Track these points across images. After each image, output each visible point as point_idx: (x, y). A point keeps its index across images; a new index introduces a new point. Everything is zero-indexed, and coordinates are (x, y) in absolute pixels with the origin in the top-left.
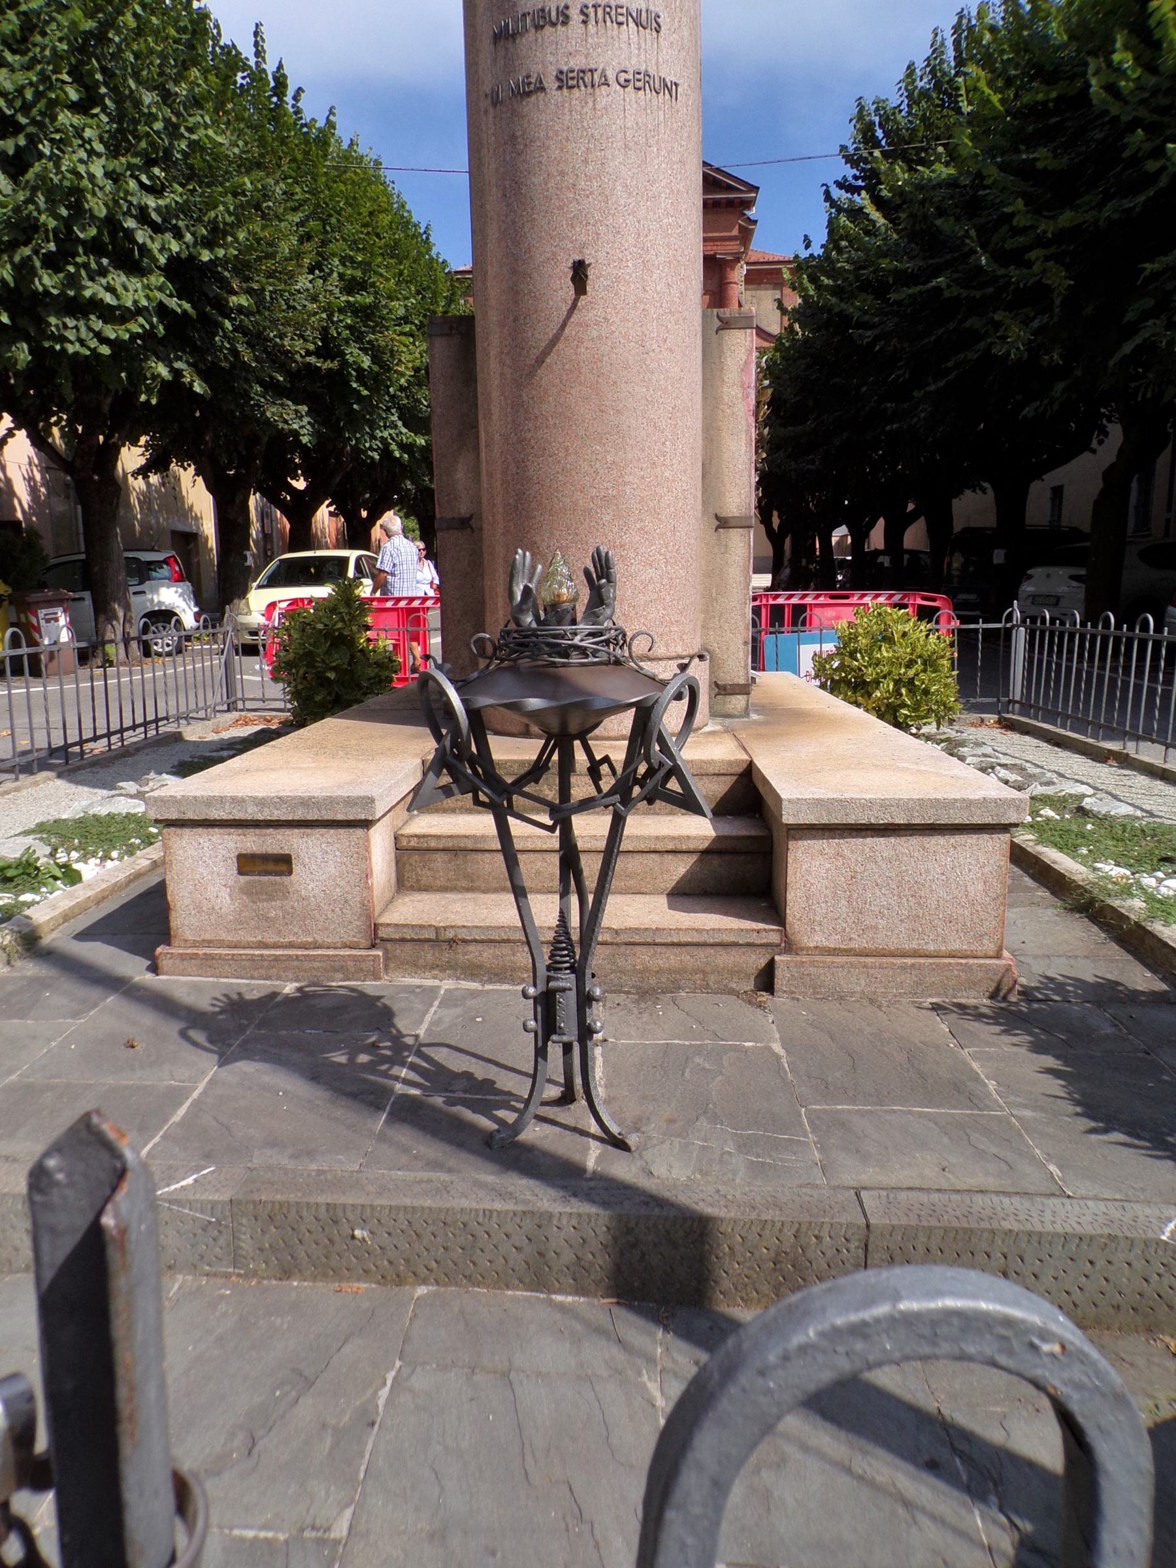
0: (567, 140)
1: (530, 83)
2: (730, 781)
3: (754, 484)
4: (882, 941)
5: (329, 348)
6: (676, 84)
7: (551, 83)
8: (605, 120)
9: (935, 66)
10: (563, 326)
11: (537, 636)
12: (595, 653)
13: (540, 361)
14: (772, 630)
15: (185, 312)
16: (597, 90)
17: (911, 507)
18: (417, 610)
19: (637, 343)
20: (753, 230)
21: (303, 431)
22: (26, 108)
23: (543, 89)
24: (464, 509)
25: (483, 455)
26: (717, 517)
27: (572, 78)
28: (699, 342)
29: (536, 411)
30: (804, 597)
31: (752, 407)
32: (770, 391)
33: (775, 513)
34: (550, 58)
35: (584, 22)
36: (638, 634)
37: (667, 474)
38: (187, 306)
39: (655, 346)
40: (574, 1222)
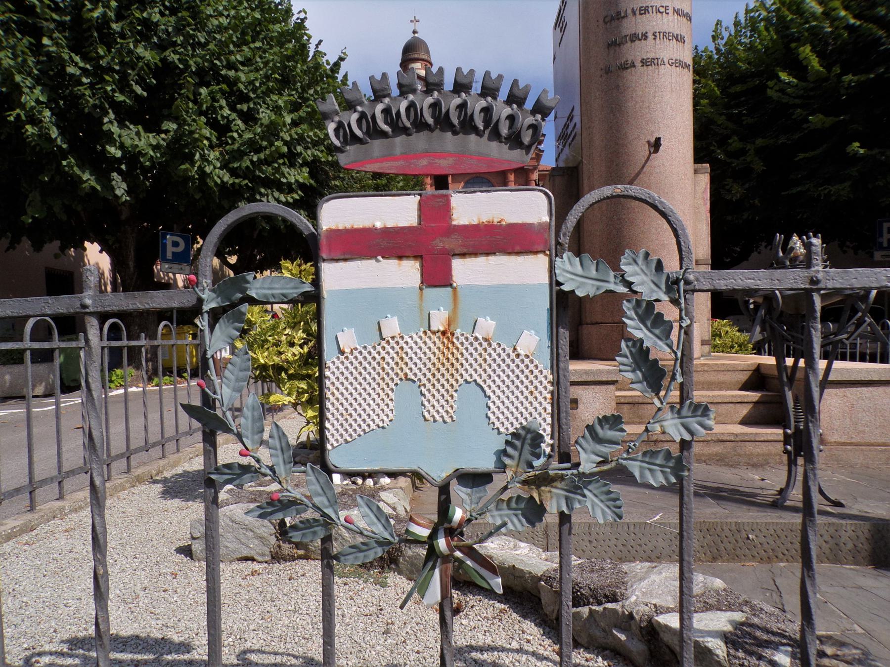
2: (749, 373)
4: (867, 439)
7: (638, 64)
15: (311, 184)
22: (254, 90)
38: (312, 182)
40: (853, 528)
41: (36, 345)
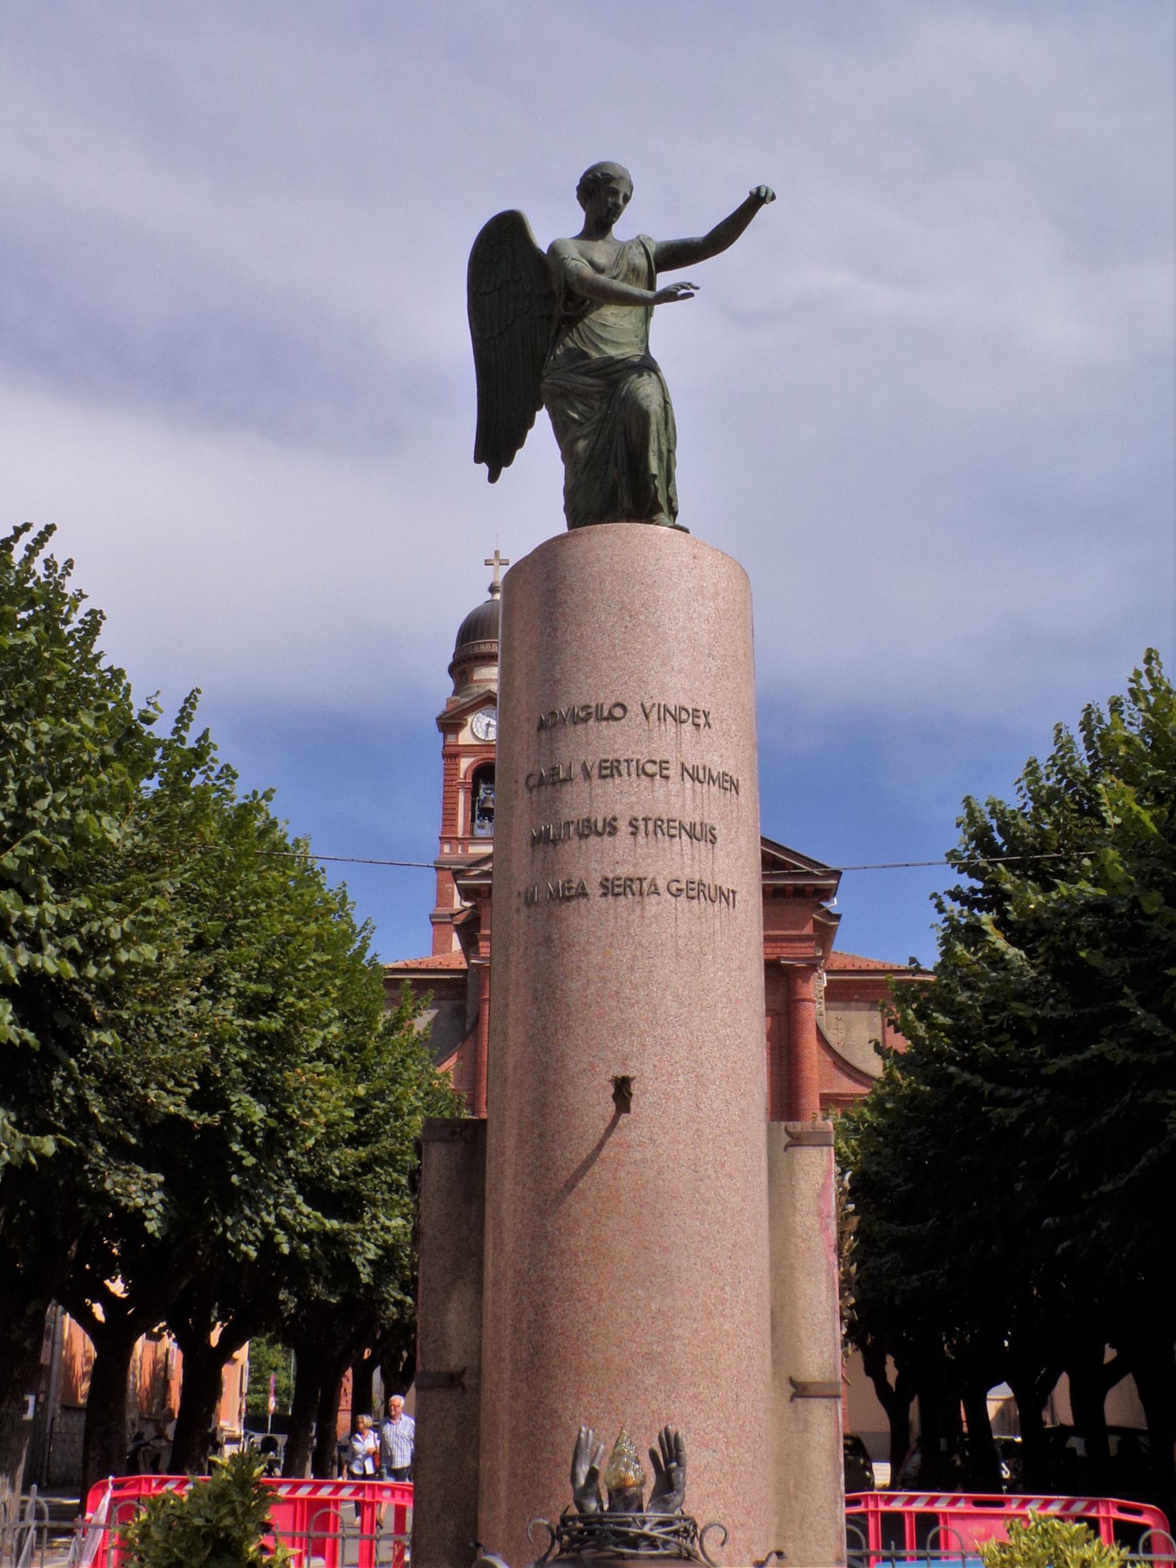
0: (611, 946)
1: (570, 889)
3: (839, 1338)
5: (209, 1097)
6: (733, 892)
7: (594, 890)
8: (654, 928)
9: (1063, 766)
10: (600, 1146)
11: (602, 1524)
12: (666, 1543)
13: (571, 1185)
14: (885, 1553)
15: (25, 1044)
16: (646, 900)
17: (1110, 1354)
18: (325, 1503)
19: (689, 1167)
20: (834, 928)
21: (150, 1214)
23: (584, 894)
24: (454, 1360)
25: (488, 1294)
26: (792, 1382)
27: (619, 886)
28: (764, 1164)
29: (563, 1245)
30: (932, 1501)
31: (834, 1242)
32: (855, 1220)
33: (890, 1360)
34: (594, 865)
35: (633, 834)
36: (711, 1525)
37: (727, 1326)
38: (29, 1036)
39: (710, 1172)
41: (55, 1524)
